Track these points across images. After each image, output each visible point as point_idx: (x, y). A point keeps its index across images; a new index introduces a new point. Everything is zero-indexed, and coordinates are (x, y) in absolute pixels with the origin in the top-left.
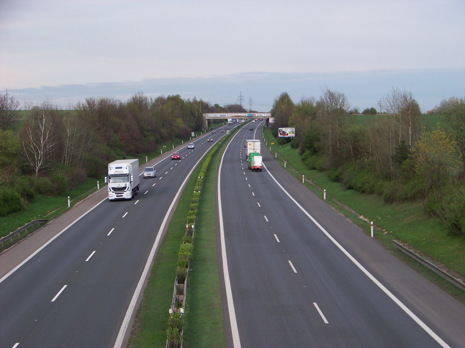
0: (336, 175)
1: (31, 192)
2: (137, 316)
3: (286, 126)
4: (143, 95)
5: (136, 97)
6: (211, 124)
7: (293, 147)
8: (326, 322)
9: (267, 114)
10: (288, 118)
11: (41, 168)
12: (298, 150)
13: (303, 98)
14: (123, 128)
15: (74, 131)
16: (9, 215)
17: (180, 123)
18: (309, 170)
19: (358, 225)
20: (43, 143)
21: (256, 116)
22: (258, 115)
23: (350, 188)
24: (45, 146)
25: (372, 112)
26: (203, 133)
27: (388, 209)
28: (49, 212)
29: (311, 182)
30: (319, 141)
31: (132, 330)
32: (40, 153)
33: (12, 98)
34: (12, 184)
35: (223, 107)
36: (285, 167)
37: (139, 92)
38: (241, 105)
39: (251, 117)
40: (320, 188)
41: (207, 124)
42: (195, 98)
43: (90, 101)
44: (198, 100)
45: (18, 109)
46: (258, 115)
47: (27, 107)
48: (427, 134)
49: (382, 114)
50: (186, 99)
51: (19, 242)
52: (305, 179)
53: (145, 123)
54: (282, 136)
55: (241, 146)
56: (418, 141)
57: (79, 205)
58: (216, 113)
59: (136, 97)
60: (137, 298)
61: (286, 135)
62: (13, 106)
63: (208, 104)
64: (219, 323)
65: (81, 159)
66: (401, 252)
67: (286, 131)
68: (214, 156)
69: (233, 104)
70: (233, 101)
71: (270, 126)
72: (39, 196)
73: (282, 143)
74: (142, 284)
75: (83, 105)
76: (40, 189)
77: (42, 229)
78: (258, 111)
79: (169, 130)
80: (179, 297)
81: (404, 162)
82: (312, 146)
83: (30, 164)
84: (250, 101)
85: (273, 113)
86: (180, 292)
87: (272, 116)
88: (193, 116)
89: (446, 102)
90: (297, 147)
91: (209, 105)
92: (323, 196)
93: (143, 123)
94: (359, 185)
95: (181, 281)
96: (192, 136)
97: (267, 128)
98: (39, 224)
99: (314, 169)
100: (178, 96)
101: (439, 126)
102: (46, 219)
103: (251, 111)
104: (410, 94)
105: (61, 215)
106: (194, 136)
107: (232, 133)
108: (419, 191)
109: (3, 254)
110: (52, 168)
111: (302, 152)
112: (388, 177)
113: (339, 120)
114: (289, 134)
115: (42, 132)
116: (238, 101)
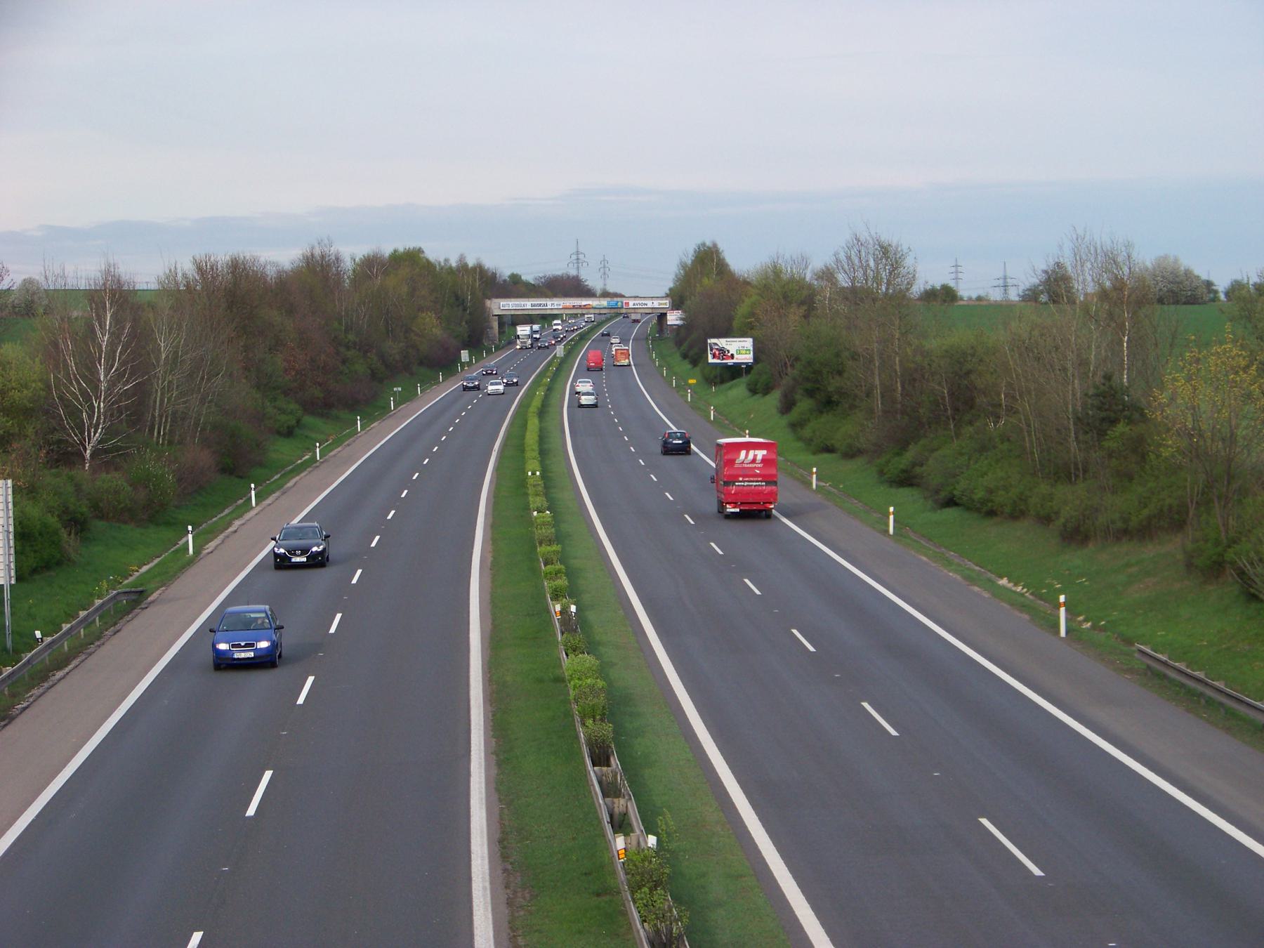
0: (902, 466)
1: (82, 515)
2: (505, 857)
3: (727, 333)
5: (312, 255)
7: (753, 390)
9: (661, 302)
10: (733, 313)
12: (774, 398)
13: (778, 258)
14: (289, 338)
15: (177, 347)
16: (37, 577)
17: (431, 327)
18: (814, 453)
19: (1012, 605)
20: (106, 376)
21: (631, 306)
22: (634, 305)
23: (951, 502)
24: (112, 384)
26: (489, 352)
27: (1076, 559)
28: (133, 568)
29: (830, 485)
30: (840, 373)
32: (96, 405)
34: (32, 492)
37: (322, 241)
38: (578, 276)
39: (615, 310)
40: (860, 502)
41: (497, 328)
42: (462, 258)
44: (471, 263)
45: (5, 287)
46: (634, 305)
49: (971, 303)
53: (340, 324)
54: (719, 361)
55: (607, 392)
57: (216, 548)
58: (518, 299)
59: (312, 255)
60: (484, 806)
64: (741, 876)
65: (197, 425)
66: (1165, 676)
67: (727, 347)
68: (542, 413)
69: (559, 273)
70: (559, 267)
71: (667, 334)
72: (100, 524)
73: (718, 380)
75: (185, 276)
76: (101, 505)
79: (401, 344)
80: (613, 803)
81: (1112, 430)
82: (818, 389)
83: (69, 435)
84: (602, 266)
85: (677, 297)
86: (610, 790)
87: (676, 306)
88: (461, 308)
89: (1147, 270)
90: (767, 390)
91: (498, 276)
92: (888, 525)
93: (336, 324)
94: (980, 494)
95: (600, 758)
96: (463, 361)
97: (660, 339)
98: (125, 601)
99: (829, 450)
100: (420, 251)
101: (1228, 333)
103: (605, 294)
105: (178, 578)
107: (570, 353)
108: (1161, 510)
110: (129, 448)
111: (787, 406)
112: (1066, 473)
113: (900, 318)
114: (736, 356)
115: (104, 349)
116: (571, 265)
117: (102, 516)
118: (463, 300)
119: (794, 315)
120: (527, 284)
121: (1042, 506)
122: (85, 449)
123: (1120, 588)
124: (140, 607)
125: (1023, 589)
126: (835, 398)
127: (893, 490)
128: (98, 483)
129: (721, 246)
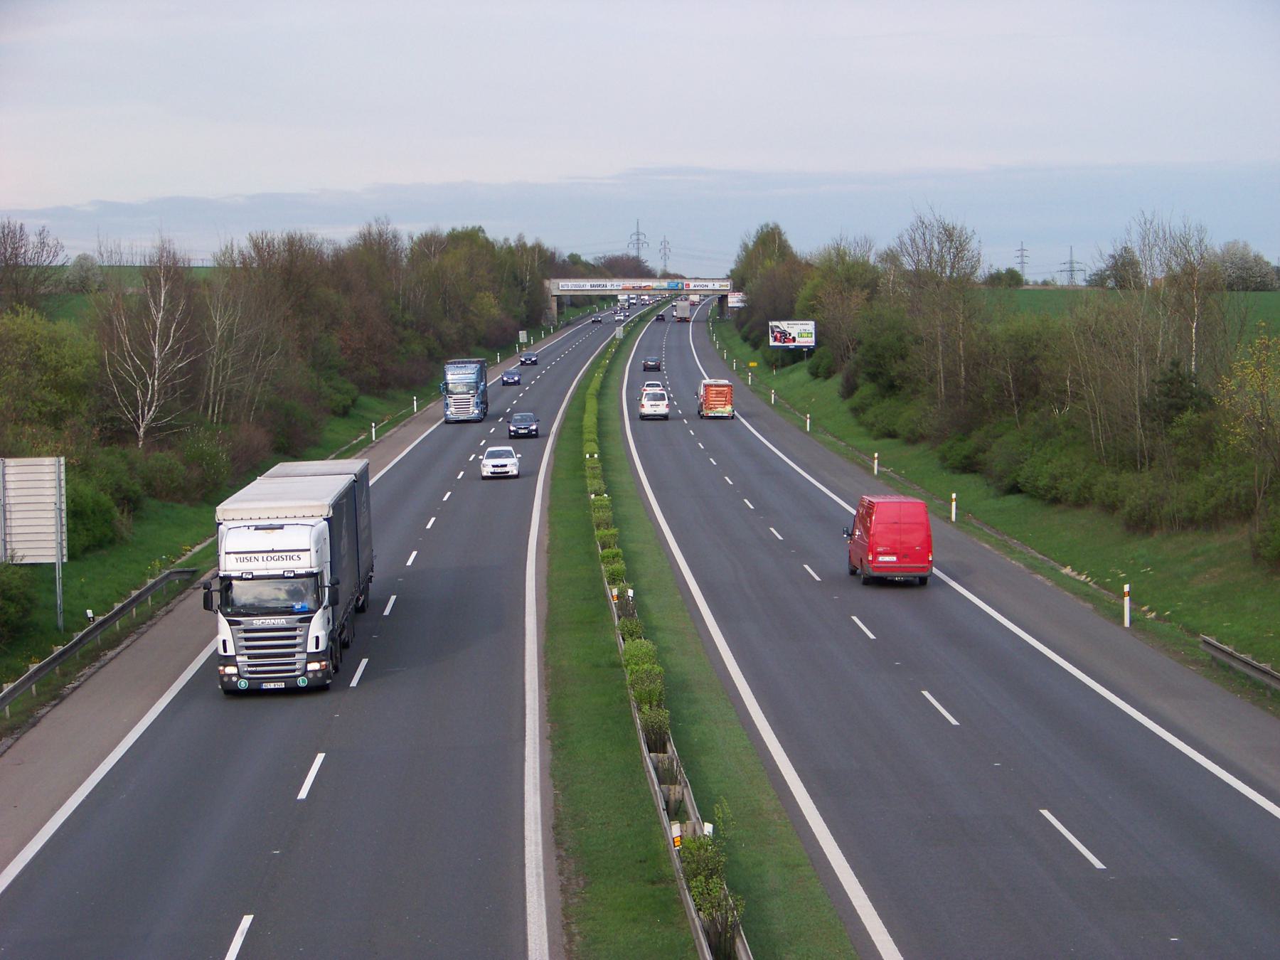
0: (964, 453)
2: (559, 844)
3: (788, 316)
4: (389, 227)
5: (370, 234)
6: (565, 310)
7: (815, 374)
8: (1099, 865)
11: (152, 425)
12: (836, 382)
13: (841, 240)
15: (232, 325)
16: (88, 555)
17: (490, 306)
18: (876, 438)
19: (1075, 594)
20: (160, 354)
22: (695, 286)
23: (1015, 489)
24: (166, 362)
25: (1012, 279)
26: (548, 333)
27: (1140, 548)
28: (186, 548)
29: (891, 471)
30: (903, 358)
31: (560, 883)
32: (150, 383)
33: (44, 230)
35: (592, 263)
36: (808, 429)
39: (676, 292)
41: (556, 308)
42: (520, 238)
43: (261, 241)
44: (530, 242)
45: (60, 263)
46: (695, 286)
47: (105, 255)
48: (1269, 340)
49: (1037, 287)
50: (501, 239)
51: (140, 630)
52: (871, 464)
53: (397, 303)
56: (1243, 361)
60: (538, 792)
61: (790, 341)
62: (45, 253)
63: (555, 254)
64: (798, 865)
65: (251, 403)
67: (789, 330)
70: (619, 247)
73: (779, 363)
74: (538, 751)
75: (241, 253)
77: (189, 595)
78: (685, 276)
80: (670, 790)
82: (880, 373)
84: (663, 246)
85: (739, 281)
86: (666, 777)
87: (737, 288)
88: (520, 288)
90: (829, 374)
91: (557, 256)
94: (1043, 482)
95: (657, 745)
96: (521, 341)
97: (722, 320)
99: (892, 435)
100: (480, 230)
102: (194, 569)
103: (666, 276)
104: (1198, 231)
106: (526, 341)
107: (630, 334)
108: (1229, 500)
109: (107, 664)
111: (849, 390)
112: (1132, 461)
114: (797, 339)
115: (158, 326)
116: (631, 246)
117: (155, 495)
118: (522, 280)
119: (858, 297)
120: (586, 264)
121: (1107, 494)
122: (139, 427)
123: (1185, 578)
124: (192, 587)
125: (1086, 578)
126: (898, 382)
127: (956, 477)
128: (151, 462)
129: (784, 227)
